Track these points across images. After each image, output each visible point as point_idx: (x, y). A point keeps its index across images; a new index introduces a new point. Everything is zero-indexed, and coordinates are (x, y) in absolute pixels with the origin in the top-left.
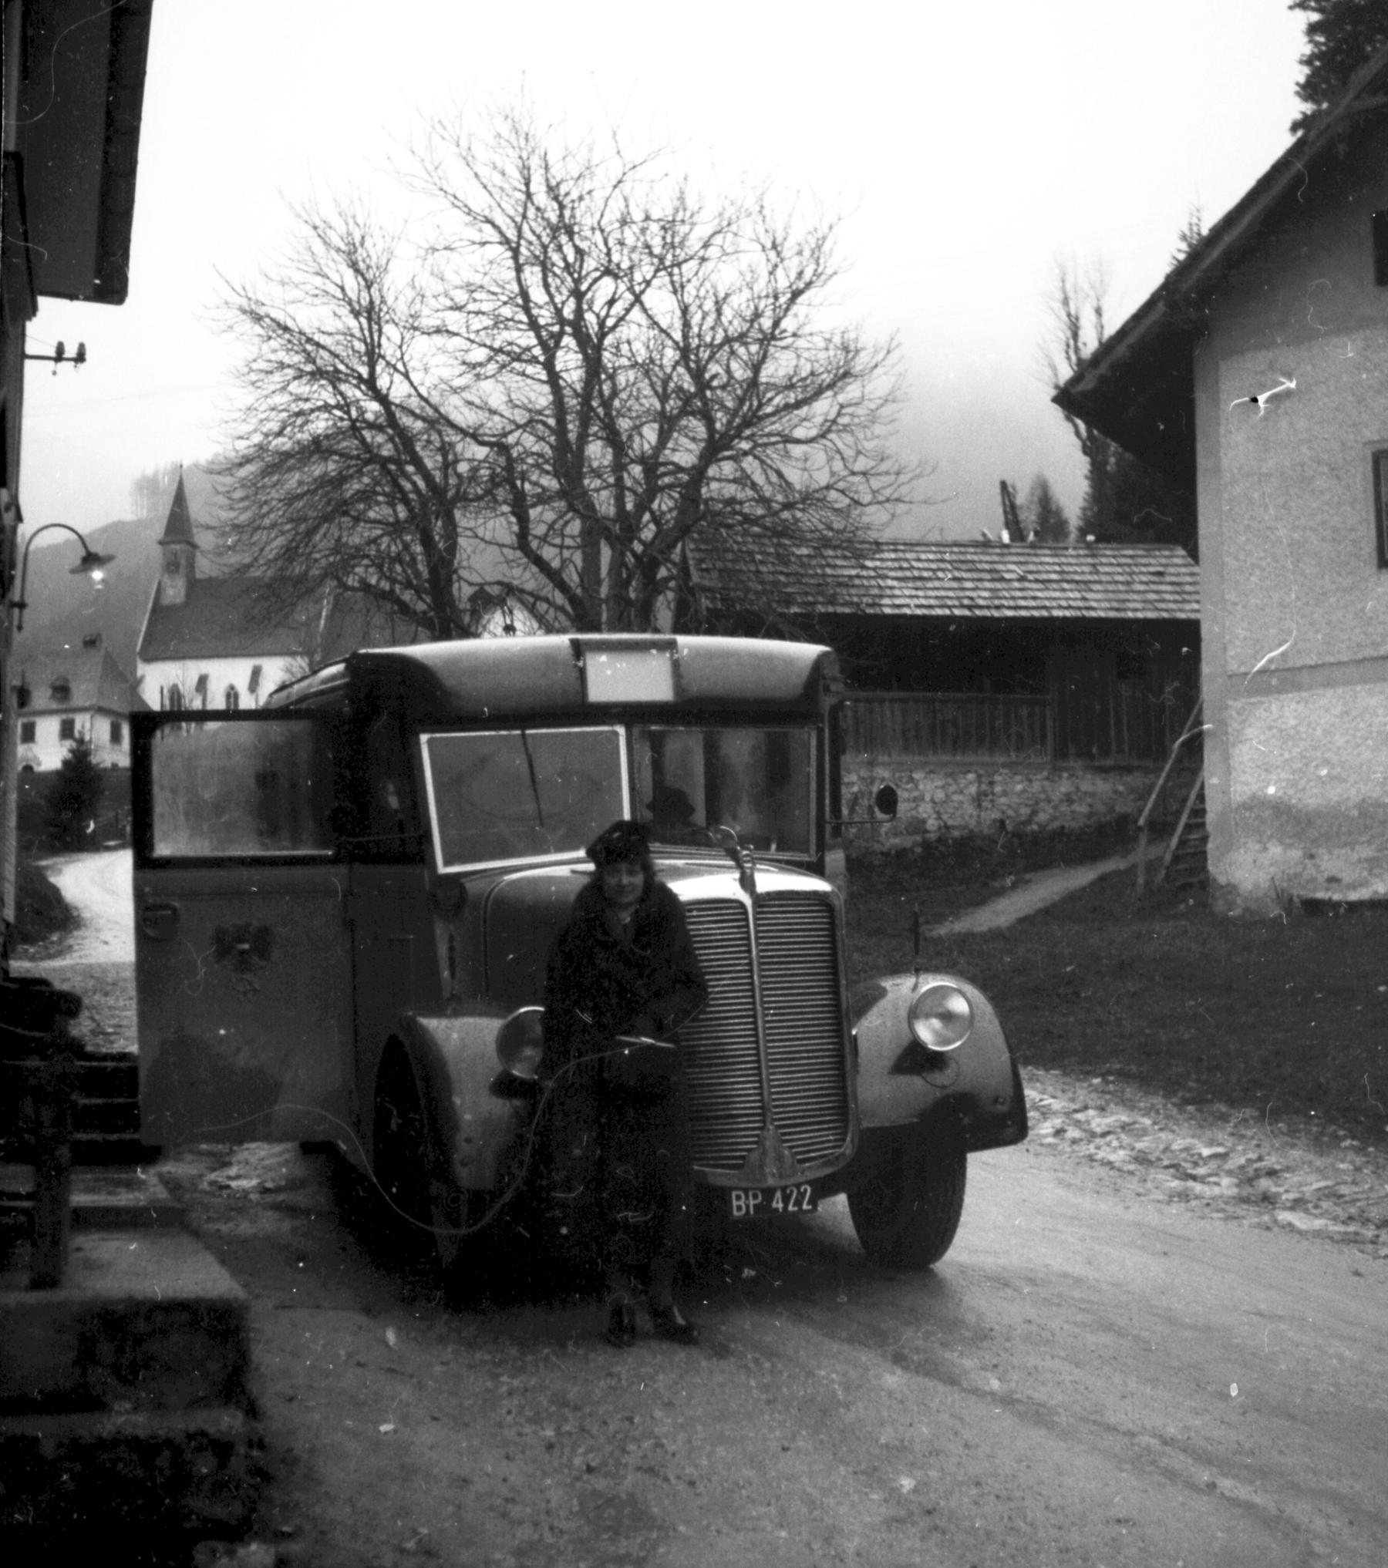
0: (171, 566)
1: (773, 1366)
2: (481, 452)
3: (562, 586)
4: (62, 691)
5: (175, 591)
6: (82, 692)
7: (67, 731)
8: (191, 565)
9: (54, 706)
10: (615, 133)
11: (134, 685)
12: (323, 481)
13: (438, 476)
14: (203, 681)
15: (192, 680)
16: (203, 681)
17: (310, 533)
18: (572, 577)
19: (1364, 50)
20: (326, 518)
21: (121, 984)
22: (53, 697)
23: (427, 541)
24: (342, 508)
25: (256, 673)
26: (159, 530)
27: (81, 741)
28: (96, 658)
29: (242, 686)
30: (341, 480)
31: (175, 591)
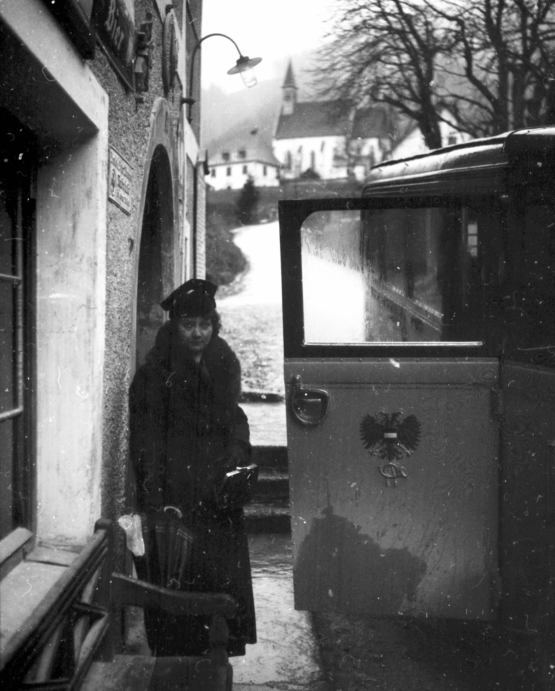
0: (287, 98)
1: (123, 100)
2: (446, 23)
3: (489, 96)
4: (242, 154)
5: (289, 109)
6: (251, 154)
7: (245, 171)
8: (295, 96)
9: (239, 160)
10: (324, 22)
11: (270, 150)
12: (368, 45)
13: (424, 37)
14: (300, 150)
15: (297, 148)
16: (300, 150)
17: (361, 71)
18: (493, 90)
19: (42, 230)
20: (367, 64)
21: (270, 323)
22: (238, 157)
23: (418, 73)
24: (376, 58)
25: (323, 144)
26: (281, 83)
27: (250, 177)
28: (256, 139)
29: (294, 153)
30: (374, 44)
31: (289, 109)
